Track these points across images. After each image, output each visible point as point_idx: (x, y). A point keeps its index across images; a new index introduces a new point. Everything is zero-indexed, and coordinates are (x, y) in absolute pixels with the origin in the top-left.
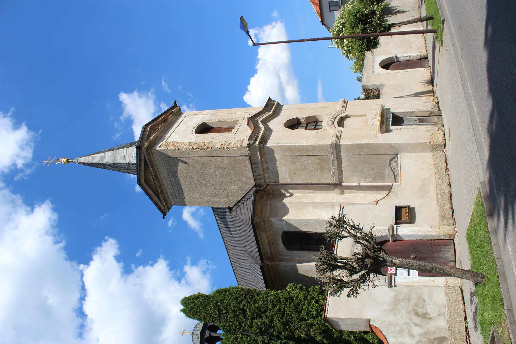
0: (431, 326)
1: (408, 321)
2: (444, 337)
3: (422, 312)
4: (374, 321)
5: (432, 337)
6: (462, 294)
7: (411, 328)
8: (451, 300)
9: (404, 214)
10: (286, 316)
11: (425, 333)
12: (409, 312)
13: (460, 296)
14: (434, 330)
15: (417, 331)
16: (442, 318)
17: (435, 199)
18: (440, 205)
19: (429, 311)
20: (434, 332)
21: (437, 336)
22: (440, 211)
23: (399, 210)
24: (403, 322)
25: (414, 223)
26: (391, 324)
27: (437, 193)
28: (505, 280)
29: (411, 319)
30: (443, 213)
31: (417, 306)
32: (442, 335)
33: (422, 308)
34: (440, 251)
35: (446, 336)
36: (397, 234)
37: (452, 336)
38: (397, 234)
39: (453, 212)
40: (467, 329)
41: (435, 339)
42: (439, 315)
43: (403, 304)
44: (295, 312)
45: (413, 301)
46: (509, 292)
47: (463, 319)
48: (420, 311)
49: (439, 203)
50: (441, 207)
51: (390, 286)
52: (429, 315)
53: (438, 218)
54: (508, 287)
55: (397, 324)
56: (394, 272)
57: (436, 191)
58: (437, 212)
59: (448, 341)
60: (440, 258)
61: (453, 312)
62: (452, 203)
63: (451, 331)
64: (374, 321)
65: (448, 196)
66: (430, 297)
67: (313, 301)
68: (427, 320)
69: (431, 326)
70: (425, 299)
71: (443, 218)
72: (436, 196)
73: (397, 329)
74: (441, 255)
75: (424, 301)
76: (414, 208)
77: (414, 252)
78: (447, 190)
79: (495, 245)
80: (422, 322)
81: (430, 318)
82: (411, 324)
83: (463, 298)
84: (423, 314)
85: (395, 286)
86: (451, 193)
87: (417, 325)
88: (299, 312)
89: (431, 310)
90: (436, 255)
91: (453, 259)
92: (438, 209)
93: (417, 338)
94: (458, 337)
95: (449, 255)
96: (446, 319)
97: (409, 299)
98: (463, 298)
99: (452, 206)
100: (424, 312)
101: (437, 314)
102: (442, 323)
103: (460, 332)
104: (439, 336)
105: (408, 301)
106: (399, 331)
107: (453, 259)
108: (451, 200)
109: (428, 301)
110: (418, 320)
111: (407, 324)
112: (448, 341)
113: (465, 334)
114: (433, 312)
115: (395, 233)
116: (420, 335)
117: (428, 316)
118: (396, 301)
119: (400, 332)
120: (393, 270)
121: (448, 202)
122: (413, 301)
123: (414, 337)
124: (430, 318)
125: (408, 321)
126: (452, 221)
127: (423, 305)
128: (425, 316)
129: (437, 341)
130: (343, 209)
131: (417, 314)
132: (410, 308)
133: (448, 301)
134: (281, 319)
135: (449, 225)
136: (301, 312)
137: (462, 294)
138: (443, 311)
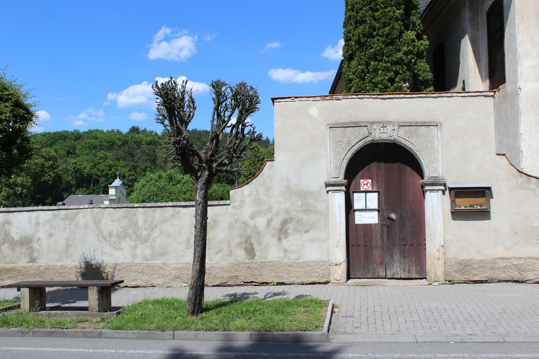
0: (269, 240)
1: (274, 211)
2: (255, 256)
3: (289, 228)
4: (271, 166)
5: (254, 241)
6: (320, 283)
7: (265, 214)
8: (309, 268)
9: (471, 202)
10: (369, 40)
11: (258, 233)
12: (287, 212)
13: (316, 280)
14: (264, 244)
15: (261, 222)
16: (282, 254)
17: (509, 255)
18: (494, 261)
19: (290, 238)
20: (261, 244)
21: (256, 247)
22: (481, 261)
23: (484, 192)
24: (272, 205)
25: (454, 219)
26: (268, 189)
27: (525, 259)
28: (140, 337)
29: (277, 214)
30: (475, 266)
31: (298, 222)
32: (258, 254)
33: (295, 229)
34: (404, 257)
35: (256, 258)
36: (427, 190)
37: (256, 265)
38: (427, 190)
39: (476, 282)
40: (267, 284)
41: (251, 244)
42: (285, 251)
43: (299, 204)
44: (375, 52)
45: (304, 217)
46: (123, 338)
47: (281, 281)
48: (290, 227)
49: (498, 261)
50: (493, 264)
51: (327, 185)
52: (285, 238)
53: (464, 256)
54: (130, 339)
55: (269, 197)
56: (362, 189)
57: (530, 258)
58: (477, 257)
59: (250, 260)
60: (391, 256)
61: (291, 268)
62: (499, 281)
63: (264, 265)
64: (271, 166)
65: (516, 275)
66: (313, 240)
67: (392, 73)
68: (278, 235)
69: (269, 240)
70: (308, 234)
71: (465, 265)
72: (518, 256)
73: (263, 197)
74: (397, 257)
75: (306, 232)
76: (490, 219)
77: (401, 217)
78: (530, 276)
79: (196, 336)
80: (275, 229)
81: (280, 239)
82: (270, 215)
83: (314, 283)
84: (286, 230)
85: (328, 192)
86: (522, 282)
87: (269, 222)
88: (375, 57)
89: (292, 241)
90: (397, 251)
91: (389, 275)
92: (485, 258)
93: (251, 223)
94: (256, 272)
95: (397, 269)
96: (279, 260)
97: (307, 211)
98: (314, 283)
99: (492, 282)
100: (289, 231)
101: (287, 248)
102: (274, 254)
103: (262, 274)
104: (256, 250)
105: (304, 211)
106: (260, 200)
107: (389, 275)
108: (507, 281)
109: (305, 237)
110: (276, 223)
111: (270, 209)
112: (250, 260)
113: (260, 280)
114: (290, 243)
115: (427, 188)
116: (255, 227)
117: (282, 237)
118: (304, 194)
119: (257, 201)
120: (365, 187)
121: (502, 276)
122: (304, 217)
123: (253, 218)
124: (280, 239)
125: (274, 211)
126: (457, 277)
127: (299, 230)
128: (282, 232)
129: (249, 247)
130: (486, 96)
131: (285, 223)
132: (294, 214)
133: (307, 264)
134: (364, 35)
135: (446, 274)
136: (376, 60)
137: (320, 283)
138: (292, 256)
